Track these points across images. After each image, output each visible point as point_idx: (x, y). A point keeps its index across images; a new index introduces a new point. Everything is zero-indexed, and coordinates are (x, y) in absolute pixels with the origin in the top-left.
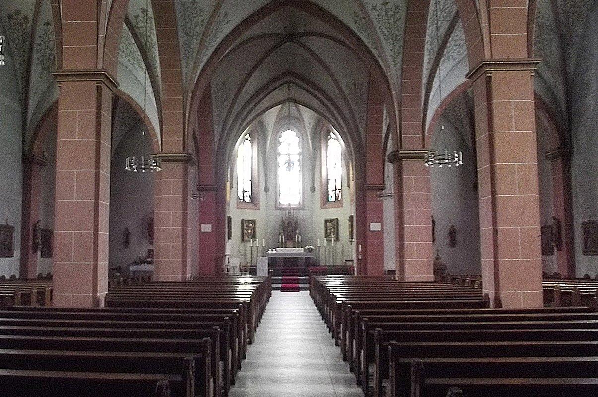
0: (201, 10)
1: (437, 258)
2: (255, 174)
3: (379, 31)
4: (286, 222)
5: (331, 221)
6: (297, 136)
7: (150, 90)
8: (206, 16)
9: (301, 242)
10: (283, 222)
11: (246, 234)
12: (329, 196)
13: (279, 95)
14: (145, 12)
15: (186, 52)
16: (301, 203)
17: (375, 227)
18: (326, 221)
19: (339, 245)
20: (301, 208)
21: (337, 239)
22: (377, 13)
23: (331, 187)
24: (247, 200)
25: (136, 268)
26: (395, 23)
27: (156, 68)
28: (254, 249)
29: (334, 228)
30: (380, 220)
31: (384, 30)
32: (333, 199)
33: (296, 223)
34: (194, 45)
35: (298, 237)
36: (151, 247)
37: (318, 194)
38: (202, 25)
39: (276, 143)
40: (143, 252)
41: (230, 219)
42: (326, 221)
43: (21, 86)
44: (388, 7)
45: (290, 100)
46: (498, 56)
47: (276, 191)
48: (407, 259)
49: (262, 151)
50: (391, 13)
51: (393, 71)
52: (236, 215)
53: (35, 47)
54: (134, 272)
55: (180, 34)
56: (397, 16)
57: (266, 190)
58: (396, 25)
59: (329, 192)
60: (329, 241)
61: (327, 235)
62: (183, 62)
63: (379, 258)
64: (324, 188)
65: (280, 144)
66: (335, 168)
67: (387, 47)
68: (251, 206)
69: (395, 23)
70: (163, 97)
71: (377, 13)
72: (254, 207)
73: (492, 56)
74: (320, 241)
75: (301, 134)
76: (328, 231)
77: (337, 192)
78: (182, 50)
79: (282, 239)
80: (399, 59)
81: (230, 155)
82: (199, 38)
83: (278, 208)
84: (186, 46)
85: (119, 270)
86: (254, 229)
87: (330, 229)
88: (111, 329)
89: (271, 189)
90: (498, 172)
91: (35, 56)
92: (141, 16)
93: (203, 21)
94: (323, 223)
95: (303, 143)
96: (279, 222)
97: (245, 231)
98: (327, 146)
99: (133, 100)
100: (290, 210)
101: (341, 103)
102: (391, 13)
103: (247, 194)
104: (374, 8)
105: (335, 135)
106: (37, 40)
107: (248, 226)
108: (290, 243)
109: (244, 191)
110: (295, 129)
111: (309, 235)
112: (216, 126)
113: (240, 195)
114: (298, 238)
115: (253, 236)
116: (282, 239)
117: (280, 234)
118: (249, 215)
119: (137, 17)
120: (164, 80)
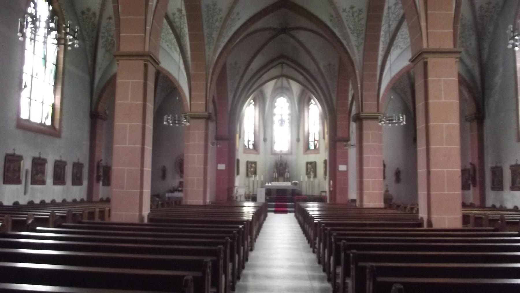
0: (220, 10)
1: (387, 191)
2: (257, 129)
4: (279, 164)
5: (311, 163)
7: (182, 67)
8: (223, 14)
11: (250, 171)
13: (275, 72)
14: (180, 10)
15: (209, 40)
17: (342, 168)
18: (307, 163)
19: (316, 181)
20: (290, 153)
21: (315, 176)
23: (311, 139)
24: (251, 147)
25: (170, 195)
27: (187, 51)
28: (256, 182)
29: (313, 168)
30: (346, 163)
31: (351, 26)
33: (286, 164)
34: (215, 35)
36: (181, 180)
38: (221, 21)
39: (273, 107)
40: (175, 183)
41: (238, 161)
43: (90, 63)
44: (354, 10)
45: (283, 76)
46: (433, 46)
51: (357, 56)
52: (242, 158)
53: (101, 35)
54: (169, 198)
56: (361, 17)
57: (265, 140)
60: (309, 177)
61: (308, 173)
62: (207, 47)
63: (345, 190)
67: (353, 39)
68: (254, 152)
69: (359, 21)
70: (192, 72)
74: (303, 177)
75: (291, 100)
76: (309, 170)
79: (275, 175)
83: (273, 153)
85: (158, 196)
86: (255, 168)
90: (431, 130)
91: (101, 41)
92: (177, 14)
93: (221, 18)
94: (305, 164)
97: (249, 170)
98: (308, 109)
102: (356, 14)
103: (251, 143)
104: (344, 11)
106: (102, 30)
107: (251, 166)
109: (249, 141)
112: (229, 93)
114: (287, 175)
115: (255, 173)
116: (275, 175)
117: (274, 172)
118: (252, 158)
119: (174, 14)
120: (193, 59)
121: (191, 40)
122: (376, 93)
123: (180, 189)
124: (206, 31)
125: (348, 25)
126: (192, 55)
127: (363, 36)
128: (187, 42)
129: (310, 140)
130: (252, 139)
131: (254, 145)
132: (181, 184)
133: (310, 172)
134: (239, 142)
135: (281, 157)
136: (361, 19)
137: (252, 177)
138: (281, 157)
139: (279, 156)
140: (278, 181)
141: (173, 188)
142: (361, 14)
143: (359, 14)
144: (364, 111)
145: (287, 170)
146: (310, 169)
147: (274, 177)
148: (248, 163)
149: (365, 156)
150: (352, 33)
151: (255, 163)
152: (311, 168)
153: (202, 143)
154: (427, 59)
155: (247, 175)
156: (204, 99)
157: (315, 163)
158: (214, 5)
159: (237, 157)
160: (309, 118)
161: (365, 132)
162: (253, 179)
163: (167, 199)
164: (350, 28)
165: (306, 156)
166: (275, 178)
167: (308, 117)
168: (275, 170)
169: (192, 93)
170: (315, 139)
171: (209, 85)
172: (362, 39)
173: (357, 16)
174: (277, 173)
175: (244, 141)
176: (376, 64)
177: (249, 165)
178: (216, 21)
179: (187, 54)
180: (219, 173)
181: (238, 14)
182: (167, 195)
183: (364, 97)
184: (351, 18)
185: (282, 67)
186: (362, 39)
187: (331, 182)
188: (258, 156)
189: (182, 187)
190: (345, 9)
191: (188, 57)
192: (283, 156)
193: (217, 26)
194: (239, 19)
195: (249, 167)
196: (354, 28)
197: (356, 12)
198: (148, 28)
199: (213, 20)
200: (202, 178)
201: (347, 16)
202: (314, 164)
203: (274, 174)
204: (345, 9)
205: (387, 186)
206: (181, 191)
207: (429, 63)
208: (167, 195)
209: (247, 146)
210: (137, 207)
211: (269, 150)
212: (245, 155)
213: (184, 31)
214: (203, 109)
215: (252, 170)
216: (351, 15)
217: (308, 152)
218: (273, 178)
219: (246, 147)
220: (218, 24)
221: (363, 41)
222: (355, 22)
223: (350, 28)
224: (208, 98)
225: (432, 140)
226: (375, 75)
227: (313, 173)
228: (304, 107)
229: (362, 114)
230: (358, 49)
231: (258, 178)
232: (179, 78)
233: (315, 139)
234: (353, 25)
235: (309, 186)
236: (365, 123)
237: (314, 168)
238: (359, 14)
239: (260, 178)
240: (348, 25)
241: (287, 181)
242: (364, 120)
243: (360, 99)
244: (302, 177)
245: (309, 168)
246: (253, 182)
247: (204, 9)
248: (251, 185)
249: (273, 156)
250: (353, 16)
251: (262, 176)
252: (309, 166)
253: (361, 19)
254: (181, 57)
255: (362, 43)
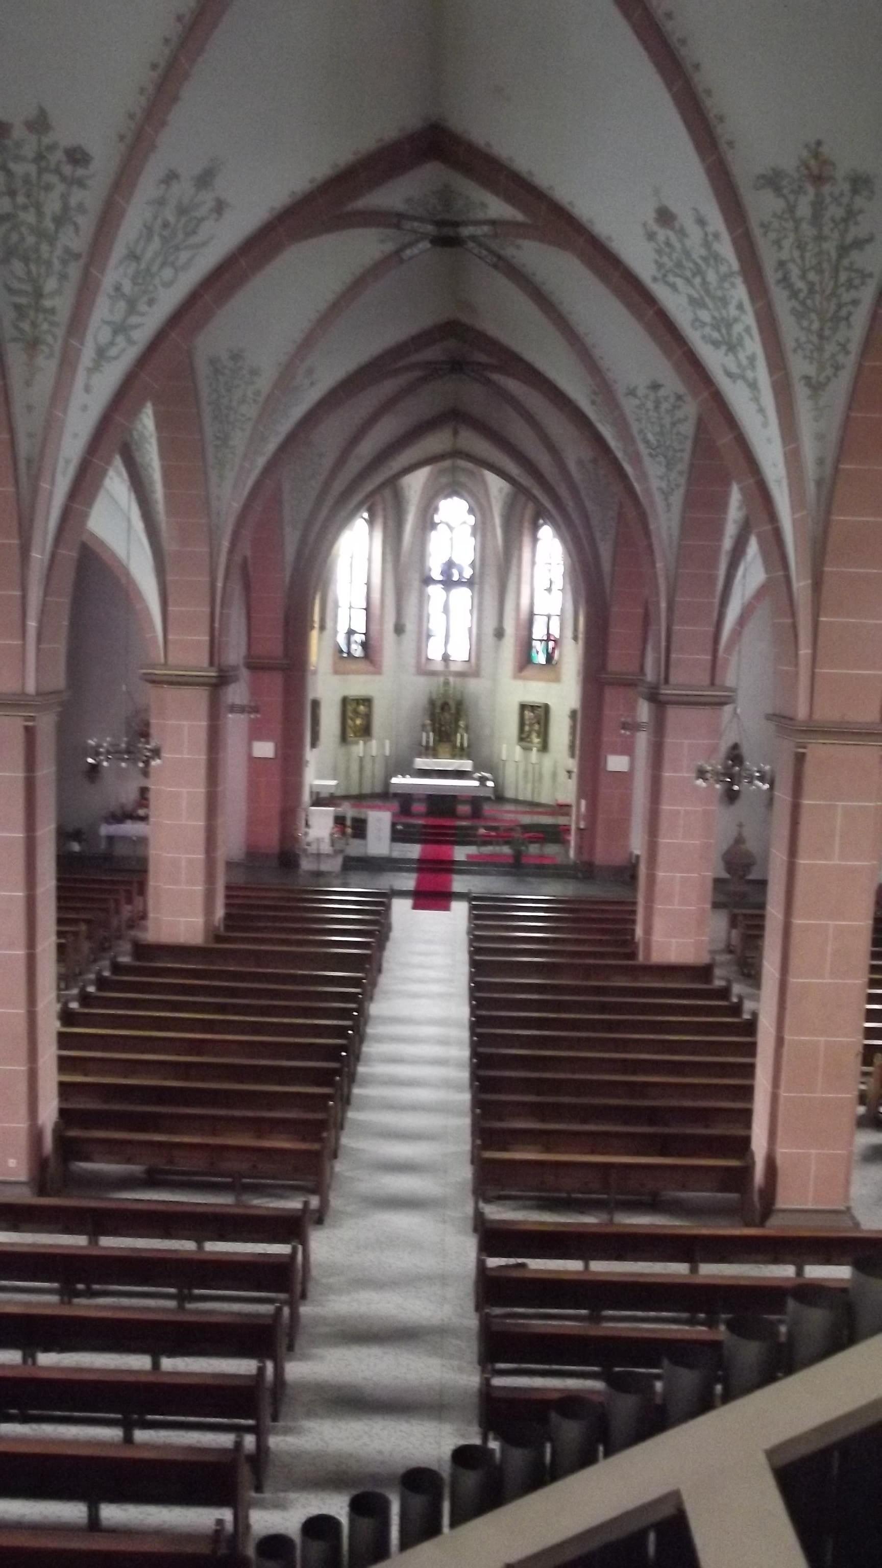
0: (254, 372)
1: (739, 840)
2: (376, 595)
3: (638, 438)
4: (439, 703)
5: (533, 708)
6: (471, 511)
7: (139, 525)
8: (264, 383)
9: (469, 746)
10: (432, 703)
11: (351, 727)
12: (534, 651)
16: (473, 660)
17: (265, 749)
18: (523, 707)
19: (548, 762)
20: (473, 670)
21: (544, 747)
22: (637, 402)
23: (539, 632)
24: (357, 651)
26: (673, 424)
27: (152, 483)
28: (368, 761)
29: (539, 723)
31: (650, 437)
32: (541, 659)
33: (460, 704)
35: (462, 737)
37: (509, 649)
39: (427, 523)
40: (128, 794)
41: (316, 704)
42: (523, 707)
44: (662, 393)
45: (456, 453)
46: (826, 713)
47: (420, 633)
48: (658, 906)
49: (393, 539)
50: (665, 406)
54: (111, 839)
55: (207, 419)
56: (680, 414)
57: (399, 629)
58: (675, 431)
59: (534, 643)
60: (527, 749)
61: (523, 737)
63: (621, 829)
64: (524, 633)
65: (434, 526)
66: (558, 564)
67: (654, 469)
68: (363, 665)
69: (673, 424)
70: (170, 546)
71: (637, 402)
72: (371, 668)
73: (800, 759)
75: (479, 508)
76: (527, 728)
77: (551, 644)
78: (210, 451)
79: (428, 737)
80: (677, 499)
81: (325, 561)
82: (74, 271)
83: (423, 669)
84: (219, 443)
85: (77, 835)
86: (368, 717)
87: (531, 725)
88: (76, 1414)
89: (410, 626)
90: (796, 937)
93: (257, 393)
94: (515, 709)
95: (481, 530)
96: (423, 701)
97: (350, 722)
98: (535, 540)
99: (102, 543)
100: (446, 673)
101: (563, 492)
102: (665, 406)
103: (359, 638)
104: (632, 393)
105: (546, 532)
107: (356, 712)
108: (444, 748)
109: (351, 632)
110: (466, 495)
111: (487, 731)
112: (288, 530)
113: (341, 640)
114: (461, 738)
115: (366, 731)
116: (428, 737)
117: (424, 726)
120: (172, 510)
121: (164, 454)
122: (711, 629)
123: (141, 812)
124: (210, 429)
125: (641, 431)
126: (168, 497)
127: (683, 466)
128: (151, 459)
129: (534, 637)
130: (360, 625)
131: (365, 645)
132: (144, 791)
133: (529, 736)
134: (320, 639)
135: (447, 683)
136: (680, 421)
137: (357, 743)
138: (447, 683)
139: (442, 679)
140: (435, 756)
141: (122, 807)
142: (679, 407)
143: (675, 407)
144: (673, 679)
145: (462, 724)
146: (531, 725)
147: (424, 743)
148: (345, 701)
149: (666, 807)
150: (651, 455)
151: (367, 701)
152: (533, 722)
153: (202, 757)
154: (805, 748)
155: (344, 738)
156: (205, 628)
157: (546, 708)
158: (236, 357)
159: (311, 695)
160: (536, 567)
161: (670, 740)
162: (359, 749)
163: (103, 845)
164: (646, 442)
165: (519, 683)
166: (427, 747)
167: (533, 563)
168: (428, 722)
169: (171, 608)
170: (548, 634)
171: (220, 584)
172: (680, 473)
173: (667, 411)
174: (434, 731)
175: (336, 632)
176: (719, 548)
177: (350, 708)
178: (243, 400)
179: (153, 492)
180: (256, 765)
181: (310, 371)
182: (105, 830)
183: (675, 639)
184: (651, 413)
185: (456, 433)
186: (680, 473)
187: (583, 803)
188: (377, 678)
189: (147, 806)
190: (636, 388)
191: (156, 502)
192: (451, 679)
193: (243, 415)
194: (312, 384)
195: (350, 714)
196: (658, 441)
197: (666, 398)
198: (32, 624)
199: (230, 401)
200: (200, 856)
201: (639, 407)
202: (541, 712)
203: (424, 735)
204: (636, 388)
205: (740, 825)
206: (144, 819)
207: (809, 758)
208: (105, 830)
209: (345, 649)
210: (23, 1110)
211: (410, 660)
212: (335, 680)
213: (144, 427)
214: (205, 663)
215: (358, 722)
216: (650, 405)
217: (526, 673)
218: (420, 744)
219: (341, 651)
220: (251, 411)
221: (683, 480)
222: (662, 426)
223: (646, 442)
224: (217, 625)
225: (795, 961)
226: (712, 580)
227: (538, 736)
228: (521, 534)
229: (663, 692)
230: (666, 499)
231: (374, 743)
232: (128, 553)
233: (548, 634)
234: (654, 434)
235: (526, 772)
236: (673, 714)
237: (542, 722)
238: (675, 407)
239: (382, 746)
240: (641, 431)
241: (461, 757)
242: (668, 706)
243: (663, 644)
244: (504, 747)
245: (527, 722)
246: (361, 759)
247: (202, 368)
248: (355, 767)
249: (422, 680)
250: (657, 407)
251: (387, 743)
252: (528, 714)
253: (680, 421)
254: (133, 496)
255: (678, 486)
